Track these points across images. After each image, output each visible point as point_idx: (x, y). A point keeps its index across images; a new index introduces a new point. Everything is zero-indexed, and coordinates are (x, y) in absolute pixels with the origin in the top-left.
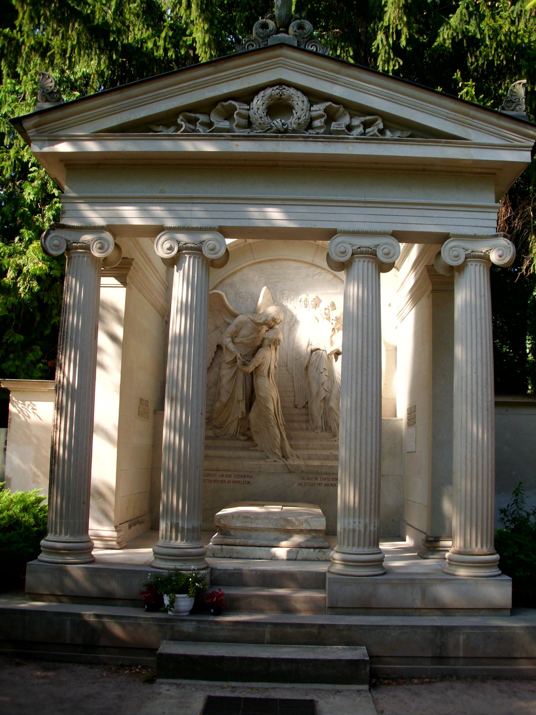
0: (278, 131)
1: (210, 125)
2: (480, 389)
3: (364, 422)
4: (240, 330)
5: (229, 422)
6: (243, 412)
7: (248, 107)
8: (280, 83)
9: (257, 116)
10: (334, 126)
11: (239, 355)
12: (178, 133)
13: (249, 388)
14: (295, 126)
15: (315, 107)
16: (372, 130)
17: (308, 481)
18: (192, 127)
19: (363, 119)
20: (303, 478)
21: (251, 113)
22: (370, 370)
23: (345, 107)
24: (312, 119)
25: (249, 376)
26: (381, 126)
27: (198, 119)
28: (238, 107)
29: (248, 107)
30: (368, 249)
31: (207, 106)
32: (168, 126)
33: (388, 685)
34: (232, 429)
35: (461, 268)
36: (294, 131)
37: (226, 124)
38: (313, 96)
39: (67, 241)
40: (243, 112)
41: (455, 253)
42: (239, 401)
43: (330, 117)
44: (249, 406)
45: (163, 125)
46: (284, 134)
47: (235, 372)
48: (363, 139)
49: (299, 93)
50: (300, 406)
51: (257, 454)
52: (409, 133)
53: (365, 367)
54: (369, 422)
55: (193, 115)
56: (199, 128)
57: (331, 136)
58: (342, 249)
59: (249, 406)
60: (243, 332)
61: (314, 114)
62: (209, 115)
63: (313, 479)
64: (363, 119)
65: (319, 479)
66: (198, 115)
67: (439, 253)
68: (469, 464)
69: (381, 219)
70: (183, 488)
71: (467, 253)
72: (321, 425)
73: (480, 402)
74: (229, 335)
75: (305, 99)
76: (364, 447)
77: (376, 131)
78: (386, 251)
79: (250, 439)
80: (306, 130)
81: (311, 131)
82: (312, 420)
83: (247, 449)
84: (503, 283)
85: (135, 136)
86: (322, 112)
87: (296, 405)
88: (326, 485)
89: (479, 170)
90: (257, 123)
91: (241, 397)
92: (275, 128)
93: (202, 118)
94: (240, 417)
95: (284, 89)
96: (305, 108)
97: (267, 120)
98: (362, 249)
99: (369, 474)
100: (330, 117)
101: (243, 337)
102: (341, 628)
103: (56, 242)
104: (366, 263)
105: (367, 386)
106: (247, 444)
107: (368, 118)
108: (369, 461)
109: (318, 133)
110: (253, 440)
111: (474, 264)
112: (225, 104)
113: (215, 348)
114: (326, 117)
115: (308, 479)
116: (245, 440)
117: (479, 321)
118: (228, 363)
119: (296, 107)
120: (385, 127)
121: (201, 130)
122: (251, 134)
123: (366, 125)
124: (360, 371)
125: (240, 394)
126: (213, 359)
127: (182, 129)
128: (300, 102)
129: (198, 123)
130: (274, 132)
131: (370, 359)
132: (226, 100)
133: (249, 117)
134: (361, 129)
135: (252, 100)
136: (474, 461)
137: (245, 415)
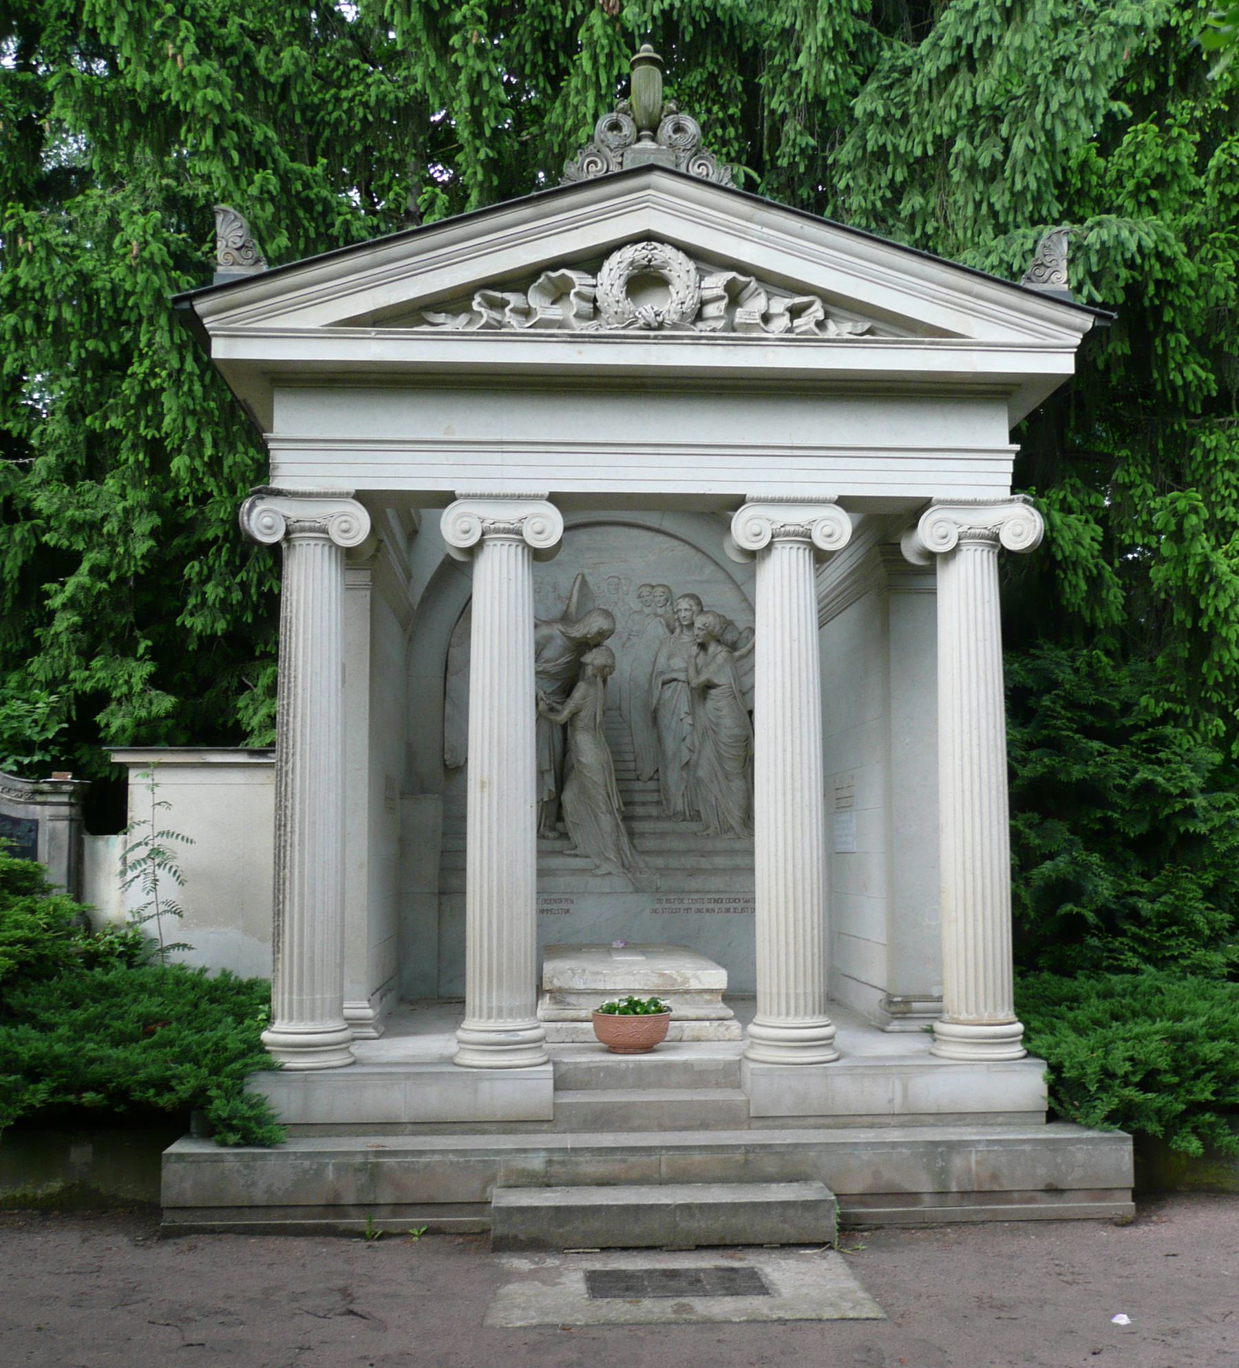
0: (648, 327)
1: (527, 313)
2: (984, 755)
3: (798, 813)
7: (593, 282)
8: (648, 237)
9: (611, 300)
10: (740, 315)
12: (474, 329)
13: (559, 748)
14: (675, 318)
15: (708, 281)
16: (805, 323)
18: (498, 316)
19: (789, 302)
20: (659, 901)
22: (805, 729)
23: (759, 279)
24: (703, 303)
27: (508, 303)
29: (593, 282)
31: (520, 280)
32: (455, 313)
36: (675, 326)
38: (703, 259)
39: (287, 518)
40: (586, 290)
41: (942, 532)
43: (734, 296)
45: (447, 312)
46: (655, 330)
48: (791, 339)
49: (681, 255)
52: (867, 326)
53: (797, 724)
54: (806, 813)
55: (498, 295)
56: (508, 316)
57: (734, 334)
61: (707, 294)
62: (526, 294)
64: (789, 302)
66: (508, 296)
68: (969, 877)
69: (819, 476)
73: (985, 775)
75: (691, 265)
76: (798, 854)
77: (812, 325)
78: (827, 530)
79: (564, 836)
80: (693, 323)
81: (700, 325)
82: (668, 800)
84: (1029, 590)
86: (720, 292)
88: (699, 911)
89: (982, 387)
90: (612, 312)
92: (642, 322)
93: (514, 299)
96: (691, 284)
97: (628, 305)
99: (808, 896)
100: (734, 296)
103: (267, 521)
104: (794, 551)
105: (801, 754)
106: (558, 845)
107: (798, 300)
108: (808, 875)
109: (714, 330)
110: (568, 838)
112: (553, 275)
114: (726, 301)
115: (668, 901)
117: (980, 644)
119: (676, 281)
120: (827, 315)
121: (513, 323)
122: (601, 332)
124: (788, 729)
128: (679, 268)
130: (641, 329)
131: (805, 711)
132: (555, 269)
133: (595, 300)
134: (785, 321)
135: (599, 268)
136: (978, 872)
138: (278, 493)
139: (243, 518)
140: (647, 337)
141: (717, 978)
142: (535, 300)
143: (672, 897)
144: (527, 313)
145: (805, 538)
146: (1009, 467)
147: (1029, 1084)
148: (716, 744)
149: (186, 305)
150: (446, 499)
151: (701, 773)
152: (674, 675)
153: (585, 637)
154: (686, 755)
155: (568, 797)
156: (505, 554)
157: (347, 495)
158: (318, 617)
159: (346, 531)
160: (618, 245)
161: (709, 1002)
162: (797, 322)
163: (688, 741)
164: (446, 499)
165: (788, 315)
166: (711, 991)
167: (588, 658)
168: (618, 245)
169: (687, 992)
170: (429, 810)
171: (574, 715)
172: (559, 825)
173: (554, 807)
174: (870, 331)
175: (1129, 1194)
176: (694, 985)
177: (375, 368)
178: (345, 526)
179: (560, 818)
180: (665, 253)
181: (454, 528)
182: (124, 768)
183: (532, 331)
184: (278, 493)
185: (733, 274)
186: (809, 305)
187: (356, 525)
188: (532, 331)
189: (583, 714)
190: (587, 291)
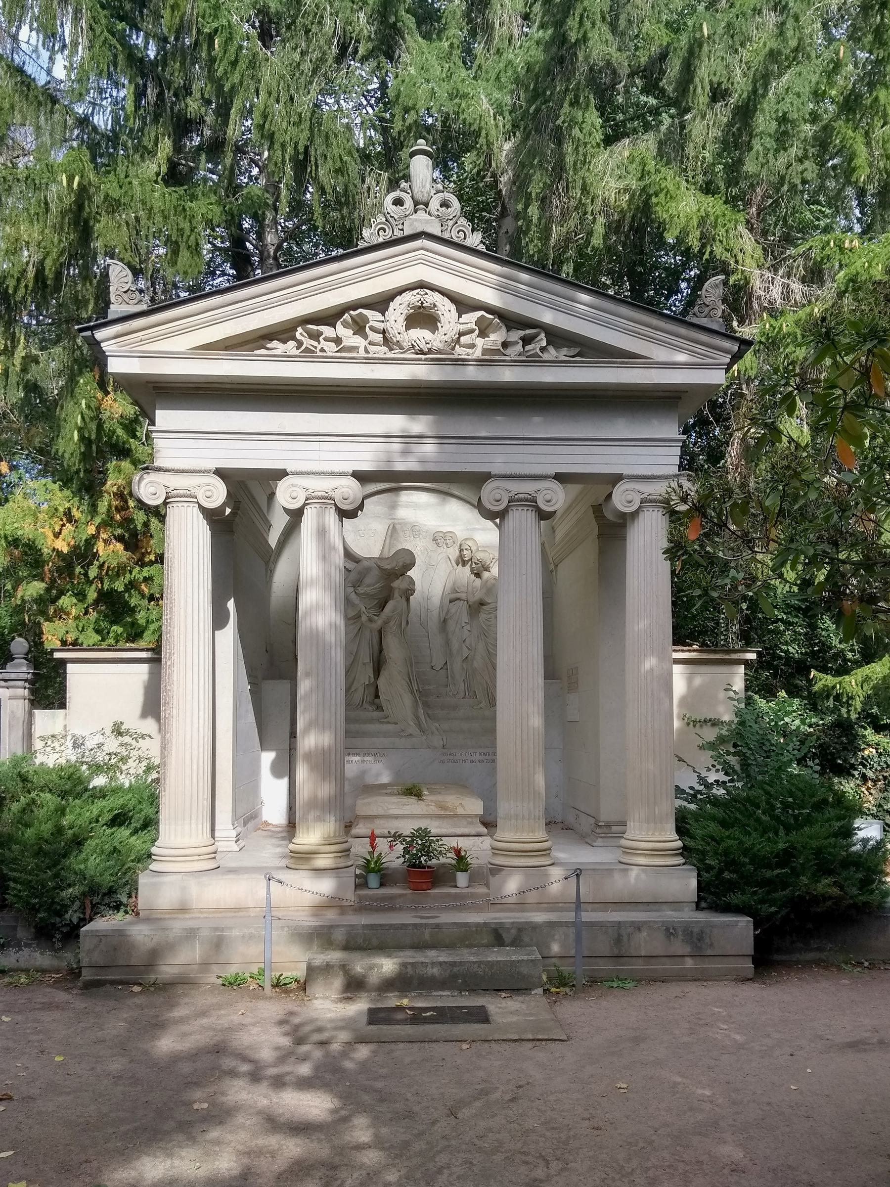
1: (338, 341)
4: (364, 577)
7: (382, 318)
8: (422, 285)
13: (376, 648)
17: (451, 758)
19: (522, 333)
21: (388, 325)
25: (377, 633)
26: (544, 343)
27: (322, 334)
28: (371, 318)
30: (527, 496)
31: (330, 317)
35: (635, 515)
37: (358, 341)
38: (463, 305)
41: (630, 498)
42: (364, 664)
44: (377, 671)
51: (390, 727)
57: (533, 361)
58: (498, 497)
59: (377, 671)
60: (368, 580)
65: (464, 754)
66: (322, 328)
67: (610, 496)
71: (642, 496)
75: (453, 307)
77: (538, 350)
78: (548, 497)
79: (379, 708)
85: (244, 355)
89: (661, 394)
91: (367, 660)
93: (327, 331)
95: (427, 294)
98: (520, 496)
102: (186, 1068)
104: (660, 513)
106: (376, 714)
107: (528, 332)
111: (651, 510)
114: (477, 332)
116: (373, 711)
123: (526, 341)
127: (303, 347)
128: (446, 309)
129: (321, 339)
133: (384, 332)
138: (160, 470)
139: (135, 488)
140: (420, 360)
141: (476, 807)
142: (341, 330)
143: (454, 751)
144: (338, 341)
145: (531, 502)
146: (678, 451)
147: (687, 883)
148: (486, 644)
149: (89, 333)
150: (282, 474)
151: (475, 664)
152: (458, 595)
153: (394, 568)
154: (466, 652)
155: (381, 682)
156: (654, 517)
157: (208, 472)
158: (188, 553)
159: (548, 501)
160: (400, 291)
161: (472, 823)
162: (527, 348)
163: (467, 642)
164: (282, 474)
165: (521, 343)
166: (470, 816)
167: (396, 584)
168: (400, 291)
169: (456, 816)
170: (276, 689)
171: (386, 622)
172: (377, 701)
173: (373, 690)
174: (578, 355)
175: (750, 959)
176: (460, 811)
177: (227, 380)
178: (209, 494)
179: (377, 696)
180: (433, 298)
181: (287, 495)
182: (63, 662)
183: (338, 354)
184: (160, 470)
185: (483, 313)
186: (536, 336)
187: (216, 494)
188: (338, 354)
189: (392, 624)
190: (380, 326)
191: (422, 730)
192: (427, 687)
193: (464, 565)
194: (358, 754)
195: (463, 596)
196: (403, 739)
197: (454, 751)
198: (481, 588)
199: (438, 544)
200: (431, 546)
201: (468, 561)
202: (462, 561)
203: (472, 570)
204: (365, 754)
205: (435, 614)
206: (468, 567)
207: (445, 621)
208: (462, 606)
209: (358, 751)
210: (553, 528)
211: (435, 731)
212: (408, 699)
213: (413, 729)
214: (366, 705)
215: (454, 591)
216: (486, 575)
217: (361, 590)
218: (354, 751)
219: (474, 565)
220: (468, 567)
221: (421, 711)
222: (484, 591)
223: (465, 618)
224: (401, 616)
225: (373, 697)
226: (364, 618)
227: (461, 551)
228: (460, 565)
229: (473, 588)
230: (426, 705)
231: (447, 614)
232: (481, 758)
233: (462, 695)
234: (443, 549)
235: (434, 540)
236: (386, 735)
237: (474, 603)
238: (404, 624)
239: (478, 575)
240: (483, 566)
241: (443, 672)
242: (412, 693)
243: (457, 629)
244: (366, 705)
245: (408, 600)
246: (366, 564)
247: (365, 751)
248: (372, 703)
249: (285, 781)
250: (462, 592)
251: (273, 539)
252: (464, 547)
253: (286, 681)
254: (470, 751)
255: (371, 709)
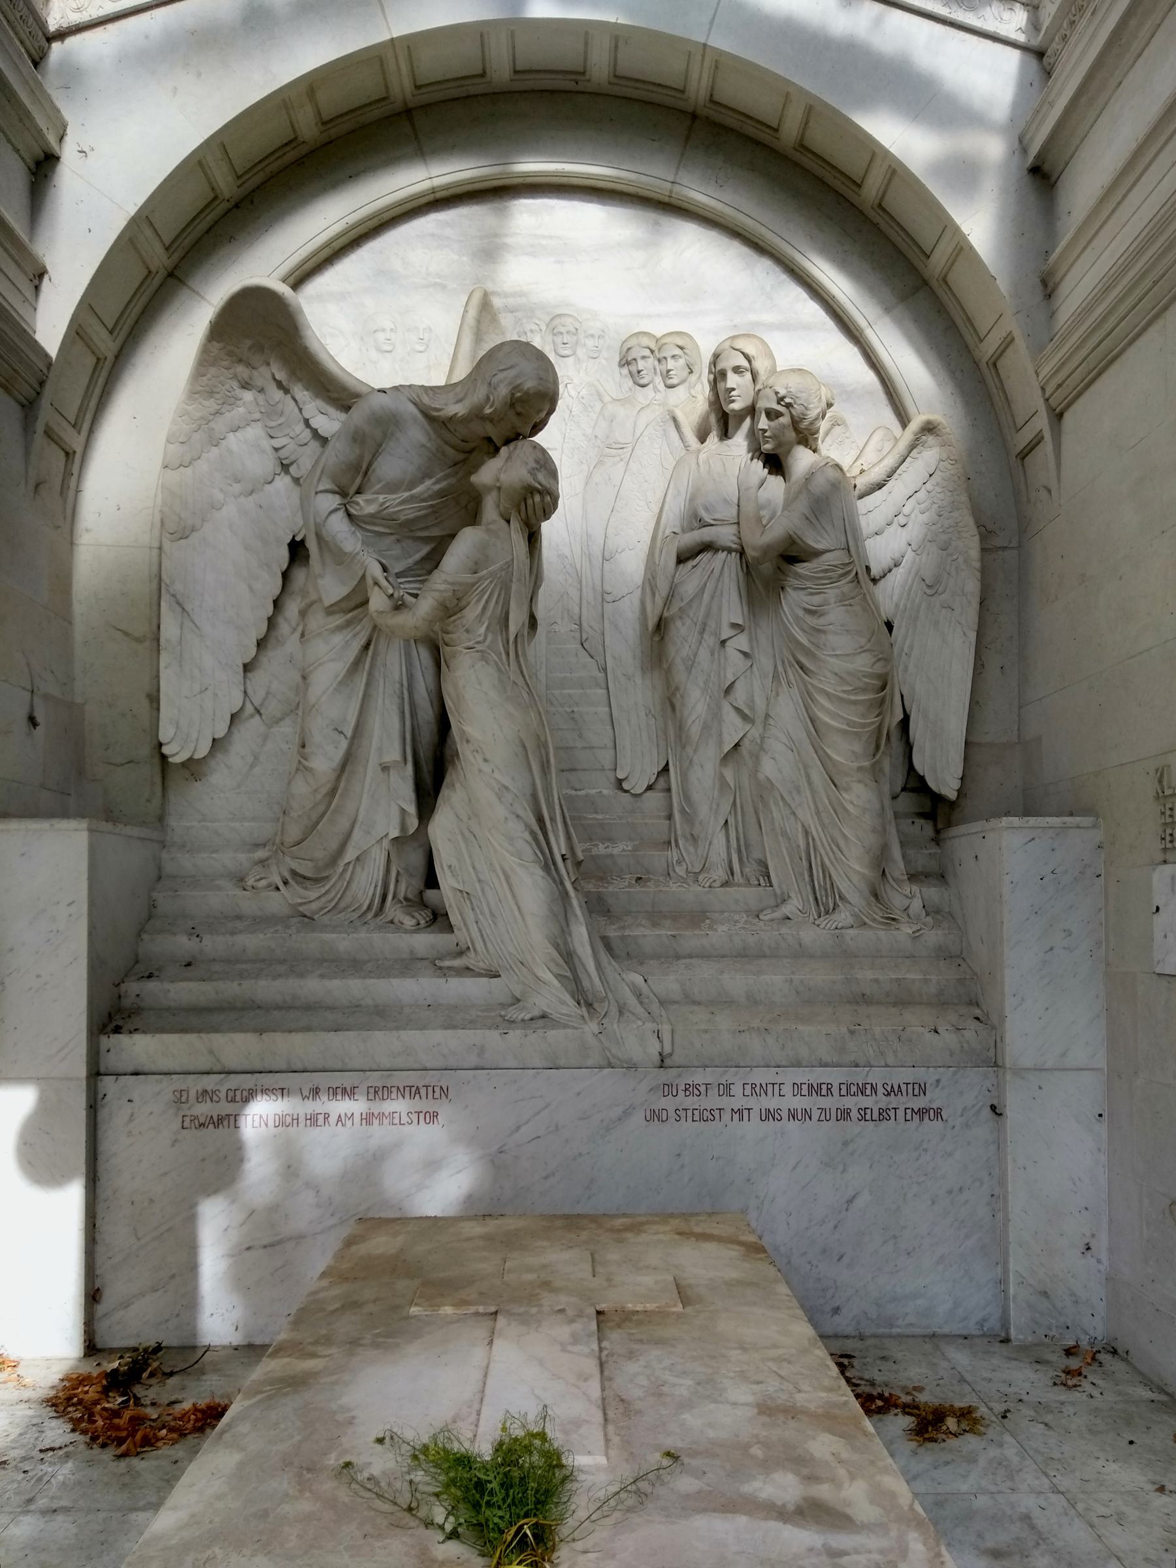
4: (374, 456)
5: (350, 855)
6: (403, 812)
11: (376, 571)
13: (427, 713)
33: (630, 1359)
34: (366, 883)
42: (385, 768)
47: (366, 647)
50: (638, 784)
51: (473, 988)
60: (393, 464)
63: (713, 1092)
65: (737, 1090)
70: (554, 809)
72: (724, 855)
74: (327, 484)
79: (438, 919)
83: (436, 965)
87: (620, 782)
94: (395, 833)
101: (392, 487)
106: (426, 941)
110: (450, 928)
113: (285, 553)
116: (418, 928)
118: (330, 611)
125: (387, 741)
126: (276, 603)
137: (413, 823)
143: (699, 1077)
151: (768, 768)
152: (706, 534)
154: (733, 729)
163: (740, 696)
171: (450, 610)
172: (430, 894)
173: (416, 859)
179: (431, 881)
189: (471, 613)
191: (584, 1000)
192: (601, 849)
193: (725, 434)
194: (348, 1092)
195: (725, 535)
196: (515, 1035)
197: (699, 1077)
198: (788, 503)
199: (636, 378)
200: (615, 382)
201: (740, 416)
202: (723, 420)
203: (756, 451)
204: (377, 1093)
205: (629, 609)
206: (739, 442)
207: (661, 627)
208: (722, 571)
209: (347, 1080)
210: (1044, 283)
211: (632, 1001)
212: (532, 889)
213: (551, 996)
214: (393, 911)
215: (696, 521)
216: (802, 460)
217: (366, 505)
218: (338, 1080)
219: (763, 423)
220: (739, 442)
221: (580, 935)
222: (802, 506)
223: (732, 609)
224: (506, 587)
225: (418, 883)
226: (378, 601)
227: (718, 377)
228: (713, 438)
229: (760, 507)
230: (598, 907)
231: (668, 601)
232: (799, 1103)
233: (720, 874)
234: (655, 397)
235: (626, 362)
236: (454, 1017)
237: (766, 550)
238: (517, 620)
239: (775, 463)
240: (795, 423)
241: (654, 800)
242: (548, 865)
243: (704, 654)
244: (393, 911)
245: (533, 538)
246: (379, 401)
247: (375, 1079)
248: (418, 902)
249: (73, 1195)
250: (722, 522)
251: (50, 324)
252: (726, 363)
253: (72, 824)
254: (761, 1076)
255: (409, 922)
